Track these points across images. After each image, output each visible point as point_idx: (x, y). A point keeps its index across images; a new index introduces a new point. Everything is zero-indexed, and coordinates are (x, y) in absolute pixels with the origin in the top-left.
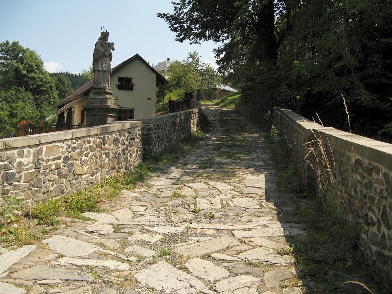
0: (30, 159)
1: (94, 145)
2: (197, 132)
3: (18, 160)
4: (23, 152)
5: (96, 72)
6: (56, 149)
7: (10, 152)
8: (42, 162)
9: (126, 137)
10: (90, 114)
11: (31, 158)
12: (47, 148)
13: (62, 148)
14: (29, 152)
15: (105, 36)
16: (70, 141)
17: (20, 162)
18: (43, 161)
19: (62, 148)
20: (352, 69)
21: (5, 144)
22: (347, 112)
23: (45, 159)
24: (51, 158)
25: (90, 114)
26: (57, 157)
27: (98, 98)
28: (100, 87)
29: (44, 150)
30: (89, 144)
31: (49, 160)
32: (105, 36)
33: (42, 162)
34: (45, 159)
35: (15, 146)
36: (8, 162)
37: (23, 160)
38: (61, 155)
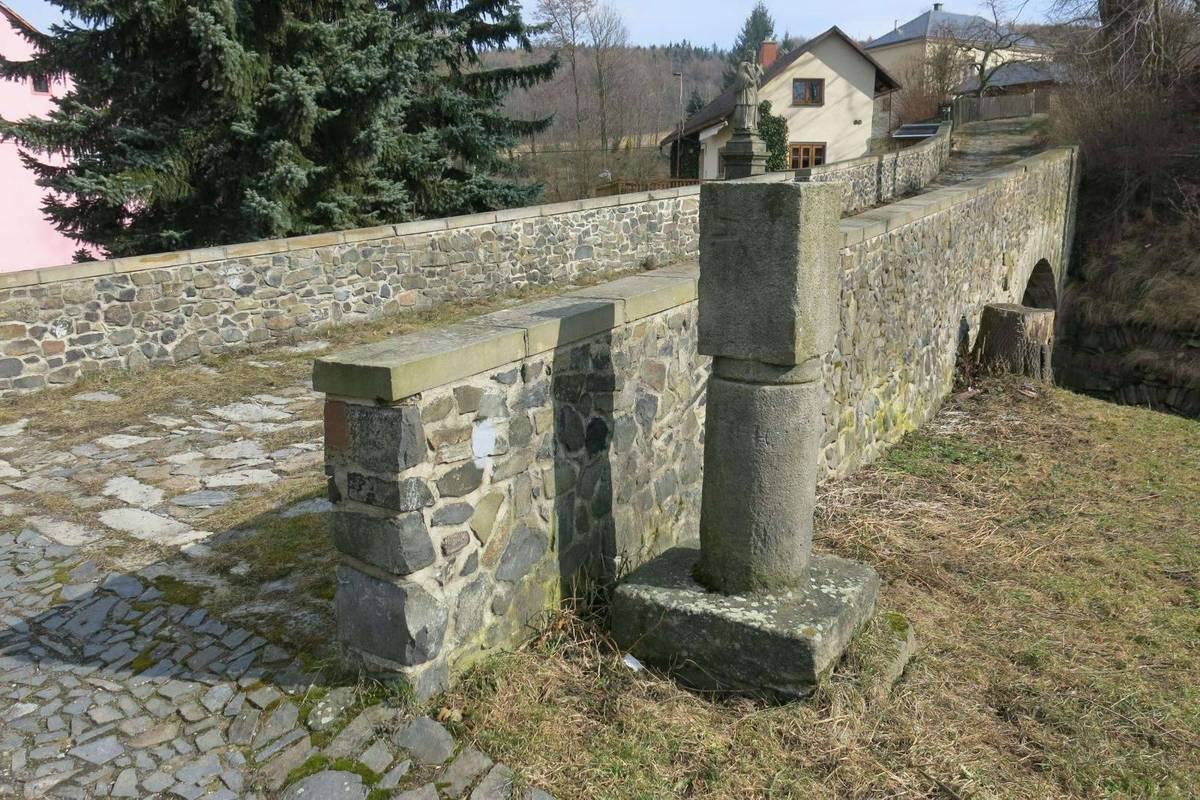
7: (652, 203)
37: (663, 211)
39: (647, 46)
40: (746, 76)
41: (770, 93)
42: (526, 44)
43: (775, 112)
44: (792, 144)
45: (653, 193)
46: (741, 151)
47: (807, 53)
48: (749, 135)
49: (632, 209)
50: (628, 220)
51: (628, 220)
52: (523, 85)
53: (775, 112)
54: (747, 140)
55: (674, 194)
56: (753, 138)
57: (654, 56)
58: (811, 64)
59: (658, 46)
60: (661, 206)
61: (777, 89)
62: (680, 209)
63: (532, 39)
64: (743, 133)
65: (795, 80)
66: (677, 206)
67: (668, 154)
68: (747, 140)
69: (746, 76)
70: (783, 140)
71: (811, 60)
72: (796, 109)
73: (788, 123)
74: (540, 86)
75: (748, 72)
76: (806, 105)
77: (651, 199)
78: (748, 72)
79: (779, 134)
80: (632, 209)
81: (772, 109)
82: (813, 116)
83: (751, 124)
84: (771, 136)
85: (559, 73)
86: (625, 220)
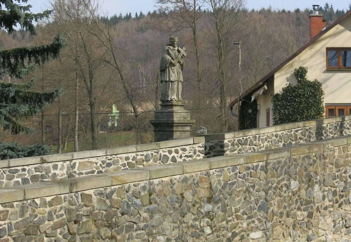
0: (64, 171)
1: (134, 162)
2: (12, 58)
3: (53, 171)
4: (57, 165)
5: (164, 83)
6: (89, 164)
7: (45, 165)
8: (75, 174)
9: (179, 155)
10: (157, 130)
11: (65, 171)
12: (80, 163)
13: (96, 163)
14: (63, 166)
15: (136, 13)
16: (104, 157)
17: (55, 174)
18: (76, 174)
19: (96, 163)
20: (71, 216)
21: (42, 159)
22: (88, 175)
23: (78, 172)
24: (84, 172)
25: (157, 130)
26: (91, 171)
27: (164, 112)
28: (167, 99)
29: (77, 165)
30: (127, 161)
31: (82, 174)
32: (136, 13)
33: (75, 174)
34: (78, 172)
35: (51, 161)
36: (44, 173)
37: (57, 172)
38: (94, 169)
39: (292, 10)
40: (168, 57)
41: (304, 61)
42: (31, 28)
43: (310, 77)
44: (328, 105)
45: (45, 157)
46: (164, 120)
47: (338, 26)
48: (172, 106)
49: (24, 170)
50: (20, 180)
51: (20, 180)
52: (37, 62)
53: (310, 77)
54: (170, 110)
55: (70, 158)
56: (175, 109)
57: (298, 19)
58: (342, 35)
59: (302, 9)
60: (55, 167)
61: (311, 57)
62: (76, 169)
63: (34, 23)
64: (167, 104)
65: (328, 49)
66: (73, 167)
67: (237, 113)
68: (170, 110)
69: (168, 57)
70: (319, 102)
71: (341, 32)
72: (329, 75)
73: (323, 87)
74: (52, 63)
75: (169, 54)
76: (339, 70)
77: (44, 162)
78: (169, 54)
79: (315, 96)
80: (24, 170)
81: (307, 74)
82: (346, 80)
83: (174, 97)
84: (308, 98)
85: (62, 52)
86: (15, 179)
